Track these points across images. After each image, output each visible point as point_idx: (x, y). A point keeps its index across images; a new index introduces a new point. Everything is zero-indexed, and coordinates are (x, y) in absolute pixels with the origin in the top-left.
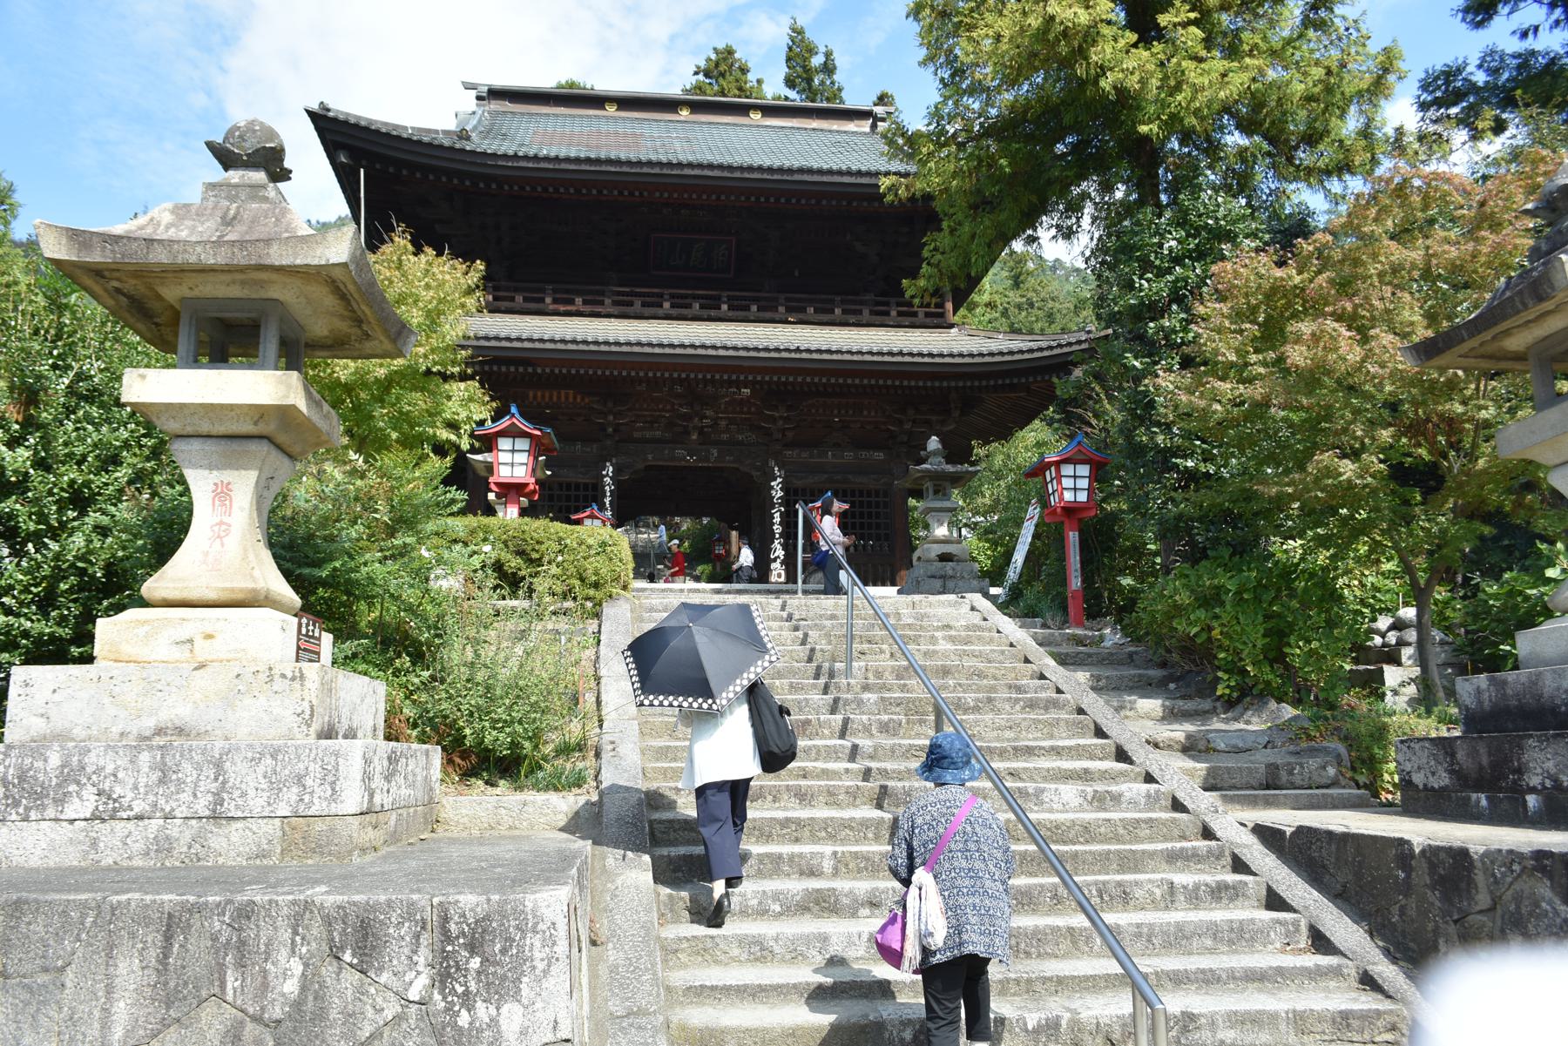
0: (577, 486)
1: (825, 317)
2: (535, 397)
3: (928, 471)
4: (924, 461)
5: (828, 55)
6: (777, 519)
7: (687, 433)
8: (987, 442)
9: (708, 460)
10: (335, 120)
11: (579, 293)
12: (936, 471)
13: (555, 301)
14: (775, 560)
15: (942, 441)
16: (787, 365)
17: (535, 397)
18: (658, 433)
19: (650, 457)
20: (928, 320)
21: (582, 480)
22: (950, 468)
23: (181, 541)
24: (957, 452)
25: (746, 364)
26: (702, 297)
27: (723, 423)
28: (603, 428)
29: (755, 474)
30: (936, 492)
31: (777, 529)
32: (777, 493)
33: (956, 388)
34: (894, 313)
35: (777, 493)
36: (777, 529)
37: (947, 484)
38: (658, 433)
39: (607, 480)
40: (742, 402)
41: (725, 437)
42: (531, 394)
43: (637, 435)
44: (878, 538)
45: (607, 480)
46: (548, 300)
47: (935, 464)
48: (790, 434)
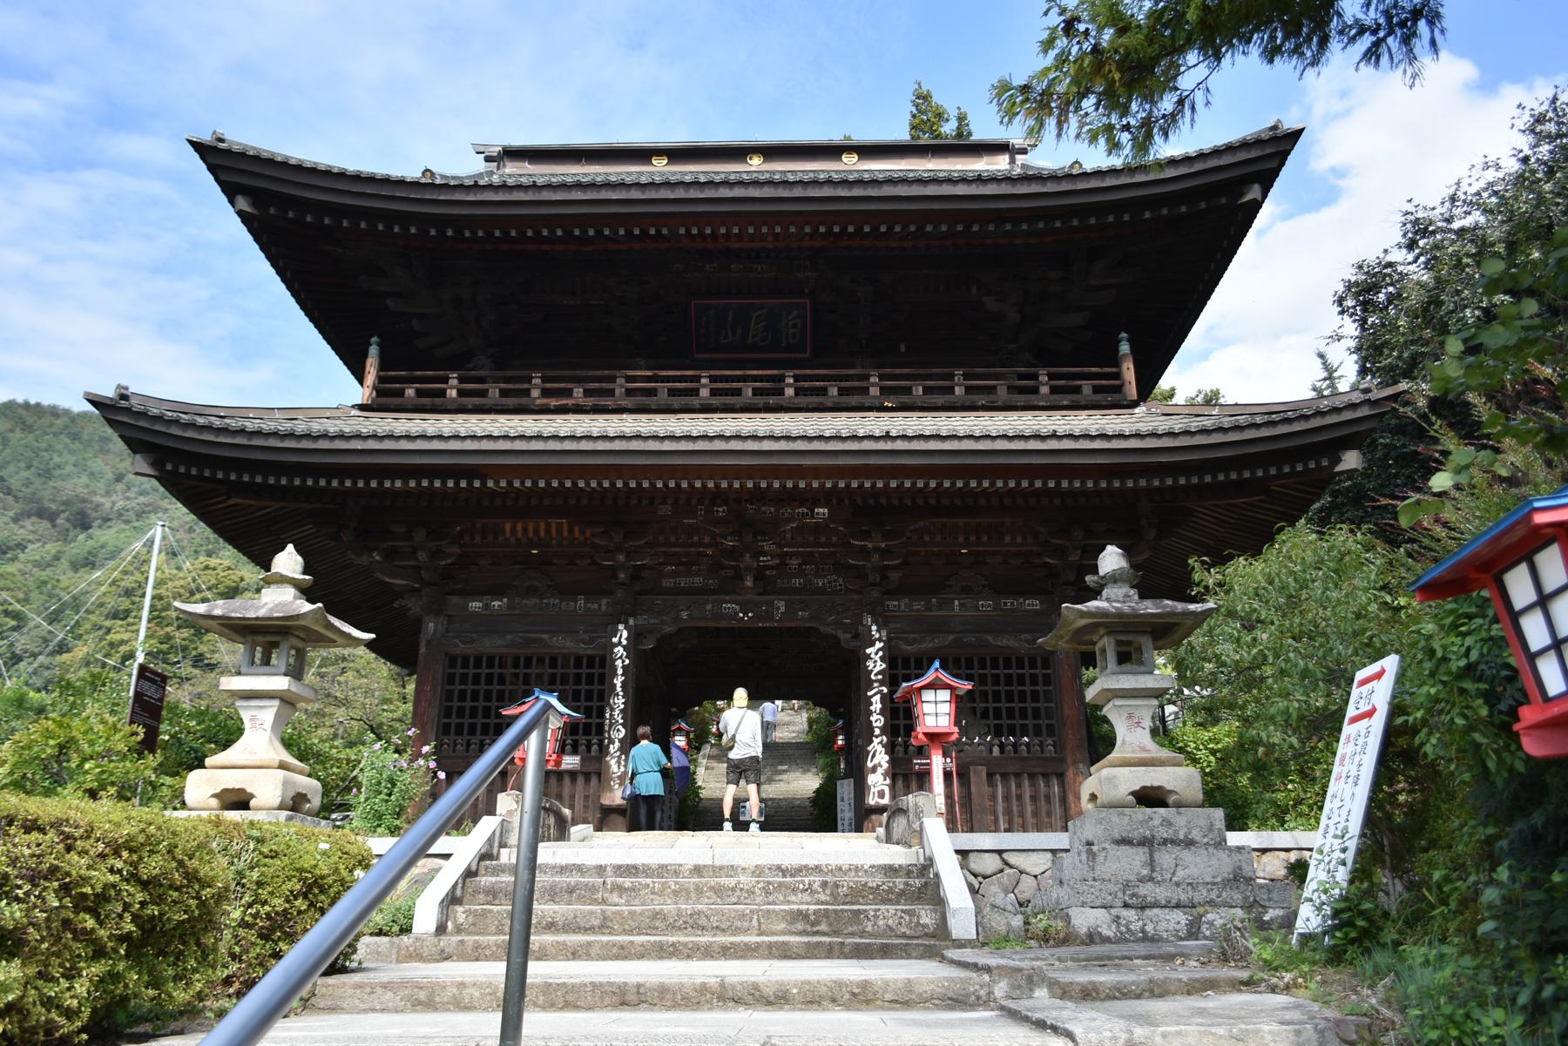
0: (578, 661)
1: (940, 400)
2: (513, 530)
3: (1102, 613)
4: (1095, 593)
5: (961, 118)
6: (876, 705)
7: (739, 577)
8: (1220, 560)
9: (770, 617)
10: (228, 152)
11: (578, 380)
12: (1120, 614)
13: (546, 393)
14: (874, 770)
15: (1128, 552)
16: (872, 461)
17: (513, 530)
18: (698, 580)
19: (684, 615)
20: (1098, 397)
21: (582, 649)
22: (1150, 607)
23: (234, 742)
24: (1154, 577)
25: (807, 461)
26: (755, 379)
27: (795, 562)
28: (613, 571)
29: (844, 637)
30: (1123, 658)
31: (877, 721)
32: (876, 664)
33: (1149, 491)
34: (1044, 390)
35: (876, 664)
36: (877, 721)
37: (1146, 642)
38: (698, 580)
39: (619, 650)
40: (818, 529)
41: (797, 582)
42: (508, 526)
43: (667, 583)
44: (1037, 732)
45: (619, 650)
46: (535, 393)
47: (1116, 600)
48: (894, 576)
